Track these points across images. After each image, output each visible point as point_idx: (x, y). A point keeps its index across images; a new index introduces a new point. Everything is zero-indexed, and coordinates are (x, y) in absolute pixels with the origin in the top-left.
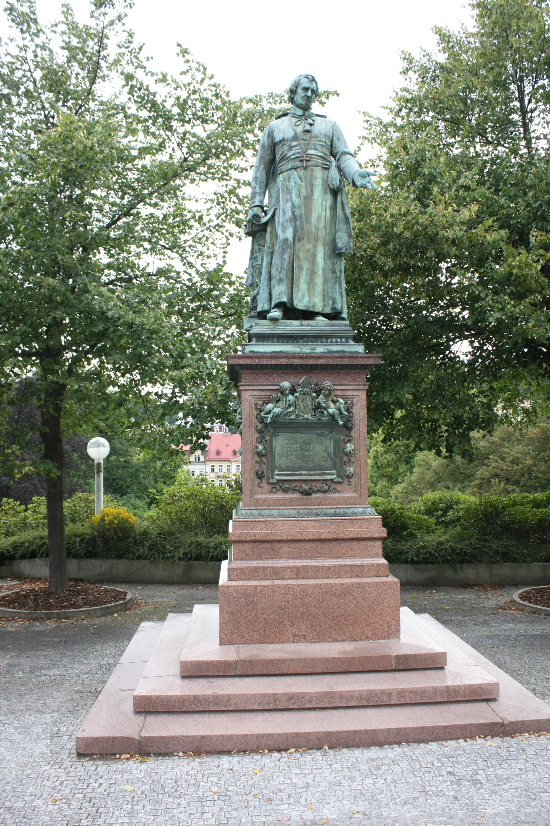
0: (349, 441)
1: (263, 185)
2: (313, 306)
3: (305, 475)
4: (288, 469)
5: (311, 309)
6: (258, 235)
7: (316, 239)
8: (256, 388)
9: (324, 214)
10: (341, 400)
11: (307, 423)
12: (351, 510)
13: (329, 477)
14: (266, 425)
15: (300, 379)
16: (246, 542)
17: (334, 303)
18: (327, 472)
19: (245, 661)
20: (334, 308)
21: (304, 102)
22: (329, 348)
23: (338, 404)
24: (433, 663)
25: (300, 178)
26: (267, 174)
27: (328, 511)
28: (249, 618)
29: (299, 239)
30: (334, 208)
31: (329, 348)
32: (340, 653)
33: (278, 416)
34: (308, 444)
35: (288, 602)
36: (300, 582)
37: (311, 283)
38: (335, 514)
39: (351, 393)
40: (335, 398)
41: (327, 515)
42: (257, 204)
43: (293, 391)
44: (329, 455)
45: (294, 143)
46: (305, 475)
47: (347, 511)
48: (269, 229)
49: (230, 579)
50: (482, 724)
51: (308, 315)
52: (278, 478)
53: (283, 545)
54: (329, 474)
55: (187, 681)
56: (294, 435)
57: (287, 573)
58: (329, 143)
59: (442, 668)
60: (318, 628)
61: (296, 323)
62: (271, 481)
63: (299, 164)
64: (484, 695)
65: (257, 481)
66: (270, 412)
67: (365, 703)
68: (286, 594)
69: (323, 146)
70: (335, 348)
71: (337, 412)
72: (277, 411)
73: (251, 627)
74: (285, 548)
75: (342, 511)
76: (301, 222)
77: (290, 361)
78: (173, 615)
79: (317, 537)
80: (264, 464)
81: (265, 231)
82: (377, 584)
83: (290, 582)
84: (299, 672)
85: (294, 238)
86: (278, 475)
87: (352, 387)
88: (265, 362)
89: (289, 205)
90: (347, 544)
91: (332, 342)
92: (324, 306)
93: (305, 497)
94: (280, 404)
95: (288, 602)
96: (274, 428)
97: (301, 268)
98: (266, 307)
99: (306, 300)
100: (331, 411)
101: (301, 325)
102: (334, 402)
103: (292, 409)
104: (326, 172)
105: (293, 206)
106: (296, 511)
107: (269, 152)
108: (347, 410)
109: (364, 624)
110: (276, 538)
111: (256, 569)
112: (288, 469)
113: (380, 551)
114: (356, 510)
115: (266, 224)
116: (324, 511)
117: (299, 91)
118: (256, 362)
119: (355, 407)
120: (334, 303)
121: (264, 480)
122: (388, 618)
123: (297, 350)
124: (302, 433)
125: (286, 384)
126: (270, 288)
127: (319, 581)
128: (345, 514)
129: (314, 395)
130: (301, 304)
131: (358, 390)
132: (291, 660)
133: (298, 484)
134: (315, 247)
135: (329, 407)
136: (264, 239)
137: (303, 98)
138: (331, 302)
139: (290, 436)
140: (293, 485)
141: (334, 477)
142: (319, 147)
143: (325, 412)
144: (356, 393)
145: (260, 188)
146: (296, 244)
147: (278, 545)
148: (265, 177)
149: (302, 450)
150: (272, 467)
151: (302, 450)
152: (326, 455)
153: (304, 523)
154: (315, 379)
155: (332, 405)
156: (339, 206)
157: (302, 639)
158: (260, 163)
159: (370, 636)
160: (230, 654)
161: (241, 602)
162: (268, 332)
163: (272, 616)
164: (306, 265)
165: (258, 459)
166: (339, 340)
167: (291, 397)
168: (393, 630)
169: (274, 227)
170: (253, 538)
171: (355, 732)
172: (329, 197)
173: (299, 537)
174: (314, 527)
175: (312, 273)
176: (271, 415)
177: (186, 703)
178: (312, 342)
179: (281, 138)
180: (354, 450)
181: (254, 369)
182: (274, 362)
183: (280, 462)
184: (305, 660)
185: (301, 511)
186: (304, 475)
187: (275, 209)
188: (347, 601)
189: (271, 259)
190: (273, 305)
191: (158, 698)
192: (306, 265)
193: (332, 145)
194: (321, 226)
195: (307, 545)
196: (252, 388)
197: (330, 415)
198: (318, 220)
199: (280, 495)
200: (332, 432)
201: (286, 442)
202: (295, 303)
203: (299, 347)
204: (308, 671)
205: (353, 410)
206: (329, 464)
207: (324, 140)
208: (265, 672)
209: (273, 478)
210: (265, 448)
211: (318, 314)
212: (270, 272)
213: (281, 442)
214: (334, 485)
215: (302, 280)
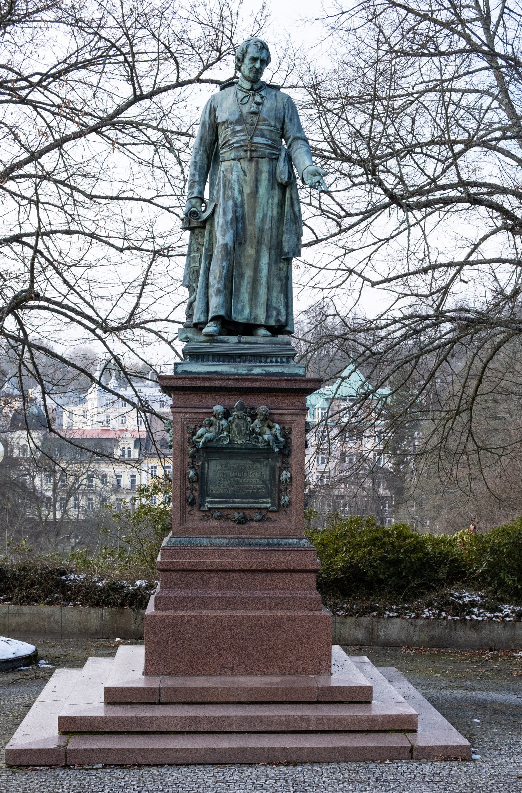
0: (285, 469)
1: (203, 172)
2: (255, 319)
3: (238, 503)
4: (220, 496)
5: (252, 322)
6: (196, 231)
7: (260, 242)
8: (188, 410)
9: (269, 213)
10: (277, 426)
11: (241, 449)
12: (285, 541)
13: (264, 506)
14: (198, 450)
15: (236, 401)
16: (174, 571)
17: (278, 314)
18: (262, 500)
19: (169, 688)
20: (278, 321)
21: (252, 75)
22: (267, 369)
23: (274, 430)
24: (362, 696)
25: (244, 171)
26: (209, 158)
27: (261, 541)
28: (176, 648)
29: (240, 244)
30: (281, 205)
31: (267, 369)
32: (265, 684)
33: (210, 441)
34: (242, 470)
35: (216, 633)
36: (228, 613)
37: (254, 293)
38: (269, 545)
39: (289, 418)
40: (271, 424)
41: (260, 545)
42: (195, 195)
43: (226, 414)
44: (264, 482)
45: (238, 128)
46: (238, 503)
47: (281, 541)
48: (208, 227)
49: (157, 608)
50: (391, 747)
51: (249, 329)
52: (209, 505)
53: (213, 574)
54: (264, 503)
55: (110, 707)
56: (228, 461)
57: (216, 604)
58: (279, 126)
59: (369, 702)
60: (246, 660)
61: (234, 339)
62: (202, 509)
63: (242, 154)
64: (406, 726)
65: (188, 508)
66: (201, 436)
67: (284, 728)
68: (214, 625)
69: (271, 131)
70: (273, 370)
71: (271, 438)
72: (208, 435)
73: (178, 658)
74: (216, 579)
75: (275, 541)
76: (244, 223)
77: (224, 384)
78: (95, 658)
79: (248, 567)
80: (196, 490)
81: (204, 227)
82: (308, 617)
83: (218, 613)
84: (223, 700)
85: (234, 243)
86: (209, 502)
87: (290, 412)
88: (198, 384)
89: (230, 203)
90: (279, 575)
91: (271, 362)
92: (268, 317)
93: (237, 526)
94: (212, 429)
95: (216, 633)
96: (207, 453)
97: (241, 276)
98: (203, 319)
99: (247, 311)
100: (266, 437)
101: (240, 342)
102: (270, 428)
103: (225, 434)
104: (275, 162)
105: (235, 205)
106: (227, 541)
107: (211, 132)
108: (284, 436)
109: (294, 658)
110: (205, 567)
111: (184, 599)
112: (220, 496)
113: (314, 584)
114: (290, 541)
115: (205, 221)
116: (257, 541)
117: (247, 61)
118: (188, 383)
119: (294, 433)
120: (278, 314)
121: (196, 508)
122: (318, 653)
123: (233, 370)
124: (236, 459)
125: (218, 408)
126: (208, 297)
127: (248, 613)
128: (278, 545)
129: (249, 419)
130: (242, 315)
131: (297, 414)
132: (215, 688)
133: (230, 512)
134: (258, 252)
135: (265, 433)
136: (203, 237)
137: (251, 70)
138: (275, 313)
139: (223, 461)
140: (225, 512)
141: (268, 505)
142: (266, 133)
143: (260, 438)
144: (294, 418)
145: (200, 176)
146: (237, 250)
147: (206, 575)
148: (206, 161)
149: (235, 477)
150: (204, 493)
151: (235, 477)
152: (261, 482)
153: (236, 553)
154: (250, 401)
155: (267, 431)
156: (287, 203)
157: (230, 672)
158: (200, 144)
159: (299, 670)
160: (156, 682)
161: (167, 632)
162: (202, 350)
163: (199, 647)
164: (248, 273)
165: (189, 485)
166: (279, 360)
167: (224, 422)
168: (324, 665)
169: (212, 225)
170: (182, 567)
171: (269, 749)
172: (277, 192)
173: (229, 567)
174: (246, 557)
175: (255, 281)
176: (203, 440)
177: (110, 724)
178: (250, 361)
179: (224, 120)
180: (291, 478)
181: (186, 390)
182: (207, 384)
183: (214, 489)
184: (230, 688)
185: (232, 541)
186: (237, 503)
187: (216, 206)
188: (277, 634)
189: (210, 263)
190: (210, 318)
191: (83, 718)
192: (248, 273)
193: (282, 128)
194: (267, 227)
195: (237, 575)
196: (183, 410)
197: (266, 441)
198: (263, 221)
199: (215, 523)
200: (267, 459)
201: (219, 467)
202: (233, 316)
203: (234, 366)
204: (232, 699)
205: (290, 436)
206: (263, 492)
207: (273, 123)
208: (189, 700)
209: (204, 506)
210: (196, 474)
211: (260, 326)
212: (207, 279)
213: (214, 468)
214: (270, 515)
215: (243, 290)
